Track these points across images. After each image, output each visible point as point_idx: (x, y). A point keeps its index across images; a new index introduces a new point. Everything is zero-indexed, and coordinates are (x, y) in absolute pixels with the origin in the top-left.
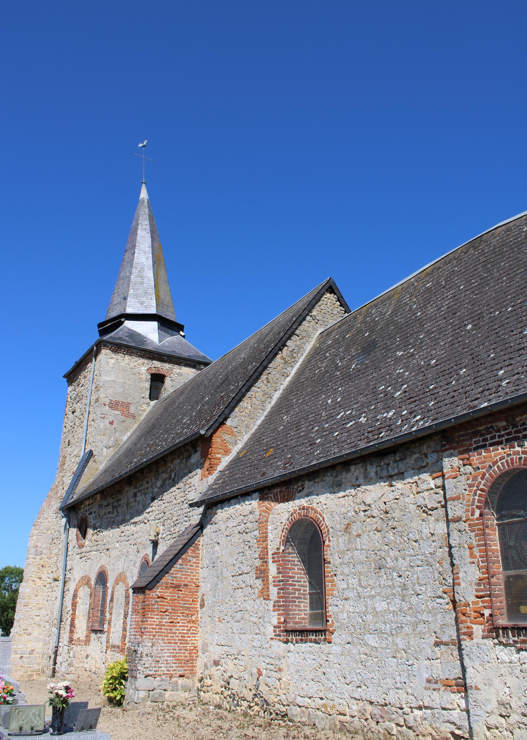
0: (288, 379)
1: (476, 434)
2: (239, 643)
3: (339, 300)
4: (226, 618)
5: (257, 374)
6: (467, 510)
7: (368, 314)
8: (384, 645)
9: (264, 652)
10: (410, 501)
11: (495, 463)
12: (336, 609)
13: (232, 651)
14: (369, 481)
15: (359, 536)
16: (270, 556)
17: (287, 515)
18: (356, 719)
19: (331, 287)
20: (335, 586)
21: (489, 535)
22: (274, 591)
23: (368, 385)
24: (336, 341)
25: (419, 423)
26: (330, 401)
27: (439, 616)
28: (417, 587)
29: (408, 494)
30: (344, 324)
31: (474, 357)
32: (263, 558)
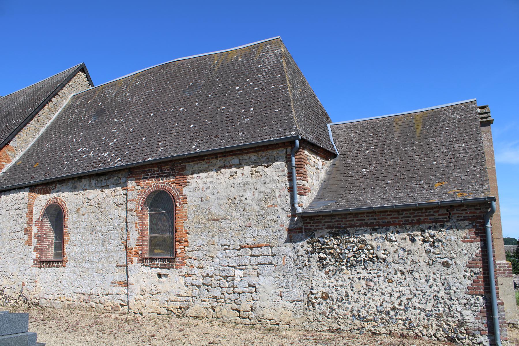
0: (51, 121)
1: (144, 171)
2: (11, 270)
3: (87, 77)
4: (3, 256)
5: (31, 116)
6: (136, 207)
7: (102, 91)
8: (92, 267)
9: (27, 273)
10: (110, 200)
11: (151, 186)
12: (69, 250)
13: (6, 274)
14: (91, 188)
15: (84, 214)
16: (34, 222)
17: (45, 201)
18: (76, 302)
19: (83, 68)
20: (69, 239)
21: (144, 218)
22: (34, 242)
23: (96, 135)
24: (82, 103)
25: (119, 163)
26: (74, 140)
27: (119, 254)
28: (110, 240)
29: (109, 196)
30: (88, 94)
31: (151, 132)
32: (29, 224)
